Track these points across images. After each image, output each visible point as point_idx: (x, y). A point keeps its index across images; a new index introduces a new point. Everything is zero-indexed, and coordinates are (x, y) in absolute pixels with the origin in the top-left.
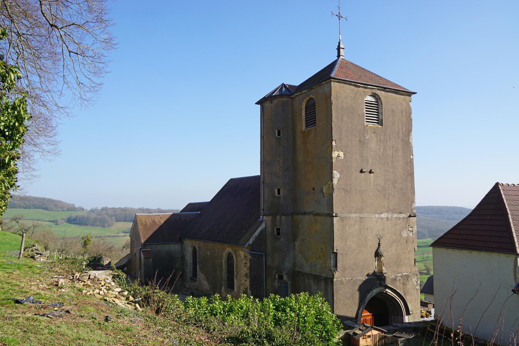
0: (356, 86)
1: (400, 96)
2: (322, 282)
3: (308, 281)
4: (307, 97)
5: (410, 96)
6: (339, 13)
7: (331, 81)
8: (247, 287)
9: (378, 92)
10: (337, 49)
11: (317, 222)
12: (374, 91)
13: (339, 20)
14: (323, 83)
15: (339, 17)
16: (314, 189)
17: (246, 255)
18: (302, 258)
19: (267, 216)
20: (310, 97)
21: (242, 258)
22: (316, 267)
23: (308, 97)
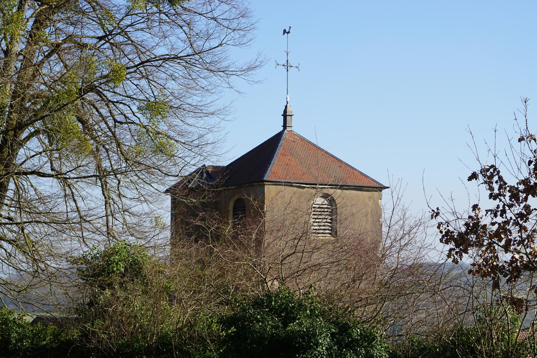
0: (299, 187)
1: (365, 193)
5: (381, 191)
6: (287, 71)
7: (264, 185)
9: (331, 191)
10: (282, 115)
12: (325, 191)
13: (287, 71)
14: (254, 184)
15: (287, 66)
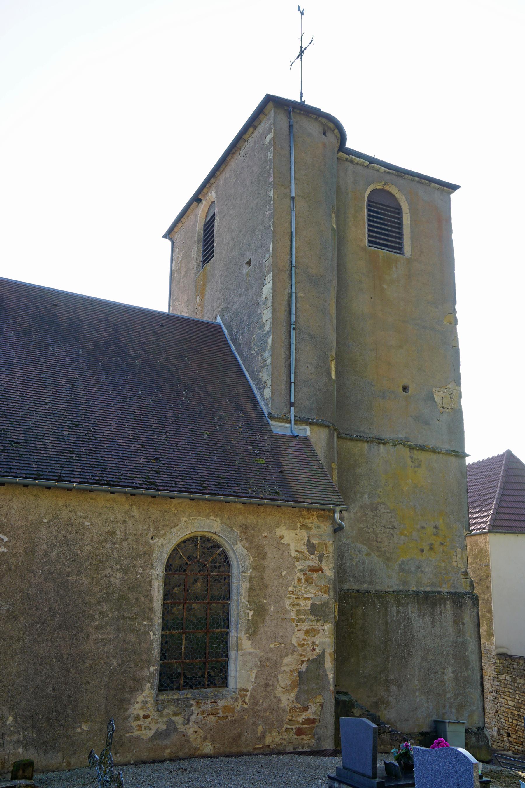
2: (445, 607)
3: (398, 612)
4: (381, 182)
8: (322, 656)
11: (419, 466)
16: (405, 389)
17: (315, 541)
18: (368, 555)
19: (315, 428)
20: (387, 188)
21: (294, 554)
22: (422, 572)
23: (383, 183)
